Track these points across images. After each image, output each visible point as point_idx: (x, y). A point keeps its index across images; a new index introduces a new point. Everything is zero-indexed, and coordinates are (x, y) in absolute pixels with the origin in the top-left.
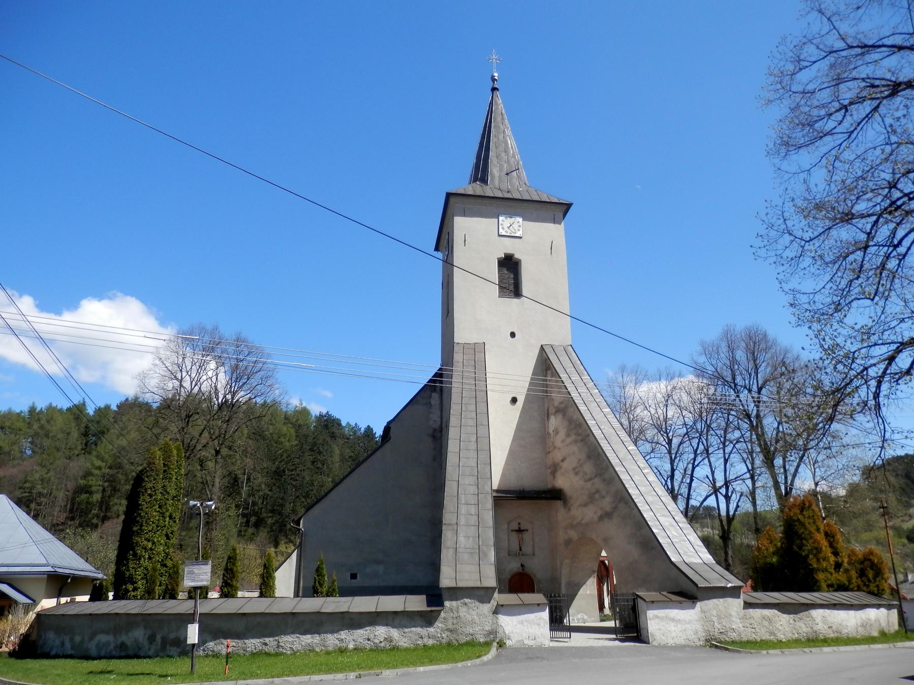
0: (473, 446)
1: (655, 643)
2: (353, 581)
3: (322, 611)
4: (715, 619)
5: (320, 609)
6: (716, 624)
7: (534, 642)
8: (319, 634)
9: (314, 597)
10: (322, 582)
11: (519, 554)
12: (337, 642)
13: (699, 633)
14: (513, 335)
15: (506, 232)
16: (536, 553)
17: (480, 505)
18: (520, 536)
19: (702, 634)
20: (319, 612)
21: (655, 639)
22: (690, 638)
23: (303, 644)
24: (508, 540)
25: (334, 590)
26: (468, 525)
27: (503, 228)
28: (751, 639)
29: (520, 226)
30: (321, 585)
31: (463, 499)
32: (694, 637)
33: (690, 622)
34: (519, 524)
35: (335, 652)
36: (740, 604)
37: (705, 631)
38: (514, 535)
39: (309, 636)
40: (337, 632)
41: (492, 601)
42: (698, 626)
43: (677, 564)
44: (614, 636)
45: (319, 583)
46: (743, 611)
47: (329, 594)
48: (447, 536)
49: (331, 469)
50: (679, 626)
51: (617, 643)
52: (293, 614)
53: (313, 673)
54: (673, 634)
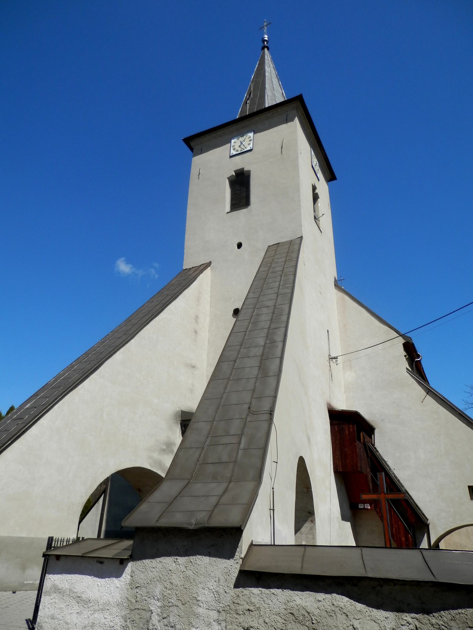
4: (155, 606)
36: (228, 574)
46: (233, 592)
50: (86, 613)
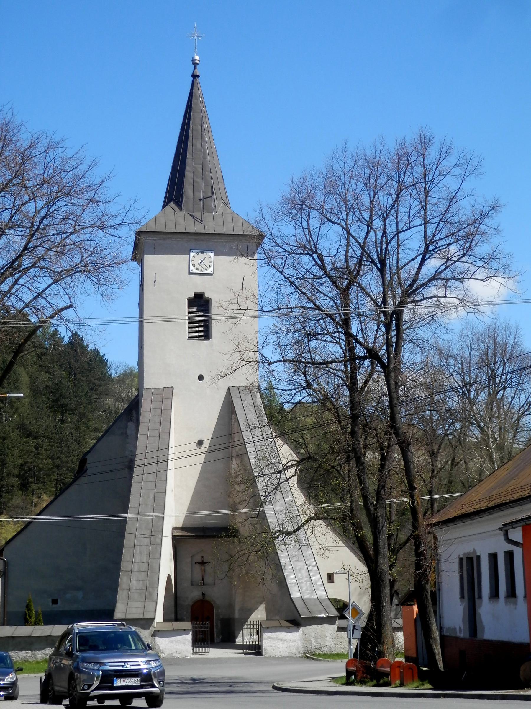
0: (150, 501)
1: (267, 655)
2: (54, 606)
3: (32, 635)
5: (31, 634)
6: (313, 642)
7: (180, 655)
8: (31, 650)
9: (26, 625)
10: (31, 615)
11: (201, 583)
12: (43, 655)
13: (300, 648)
14: (201, 378)
15: (197, 269)
16: (216, 583)
17: (151, 555)
18: (203, 568)
19: (301, 649)
20: (30, 636)
21: (267, 653)
22: (293, 652)
23: (21, 657)
24: (192, 571)
25: (40, 620)
26: (140, 571)
27: (194, 265)
28: (339, 652)
29: (211, 262)
30: (30, 617)
31: (138, 549)
32: (295, 651)
33: (293, 641)
34: (202, 557)
35: (42, 662)
36: (334, 629)
37: (304, 647)
38: (198, 568)
39: (24, 652)
40: (43, 649)
41: (151, 628)
42: (300, 644)
43: (294, 600)
44: (241, 651)
45: (29, 615)
46: (336, 633)
47: (36, 624)
48: (123, 580)
49: (17, 409)
50: (286, 644)
51: (243, 655)
52: (13, 638)
53: (30, 673)
54: (281, 649)
